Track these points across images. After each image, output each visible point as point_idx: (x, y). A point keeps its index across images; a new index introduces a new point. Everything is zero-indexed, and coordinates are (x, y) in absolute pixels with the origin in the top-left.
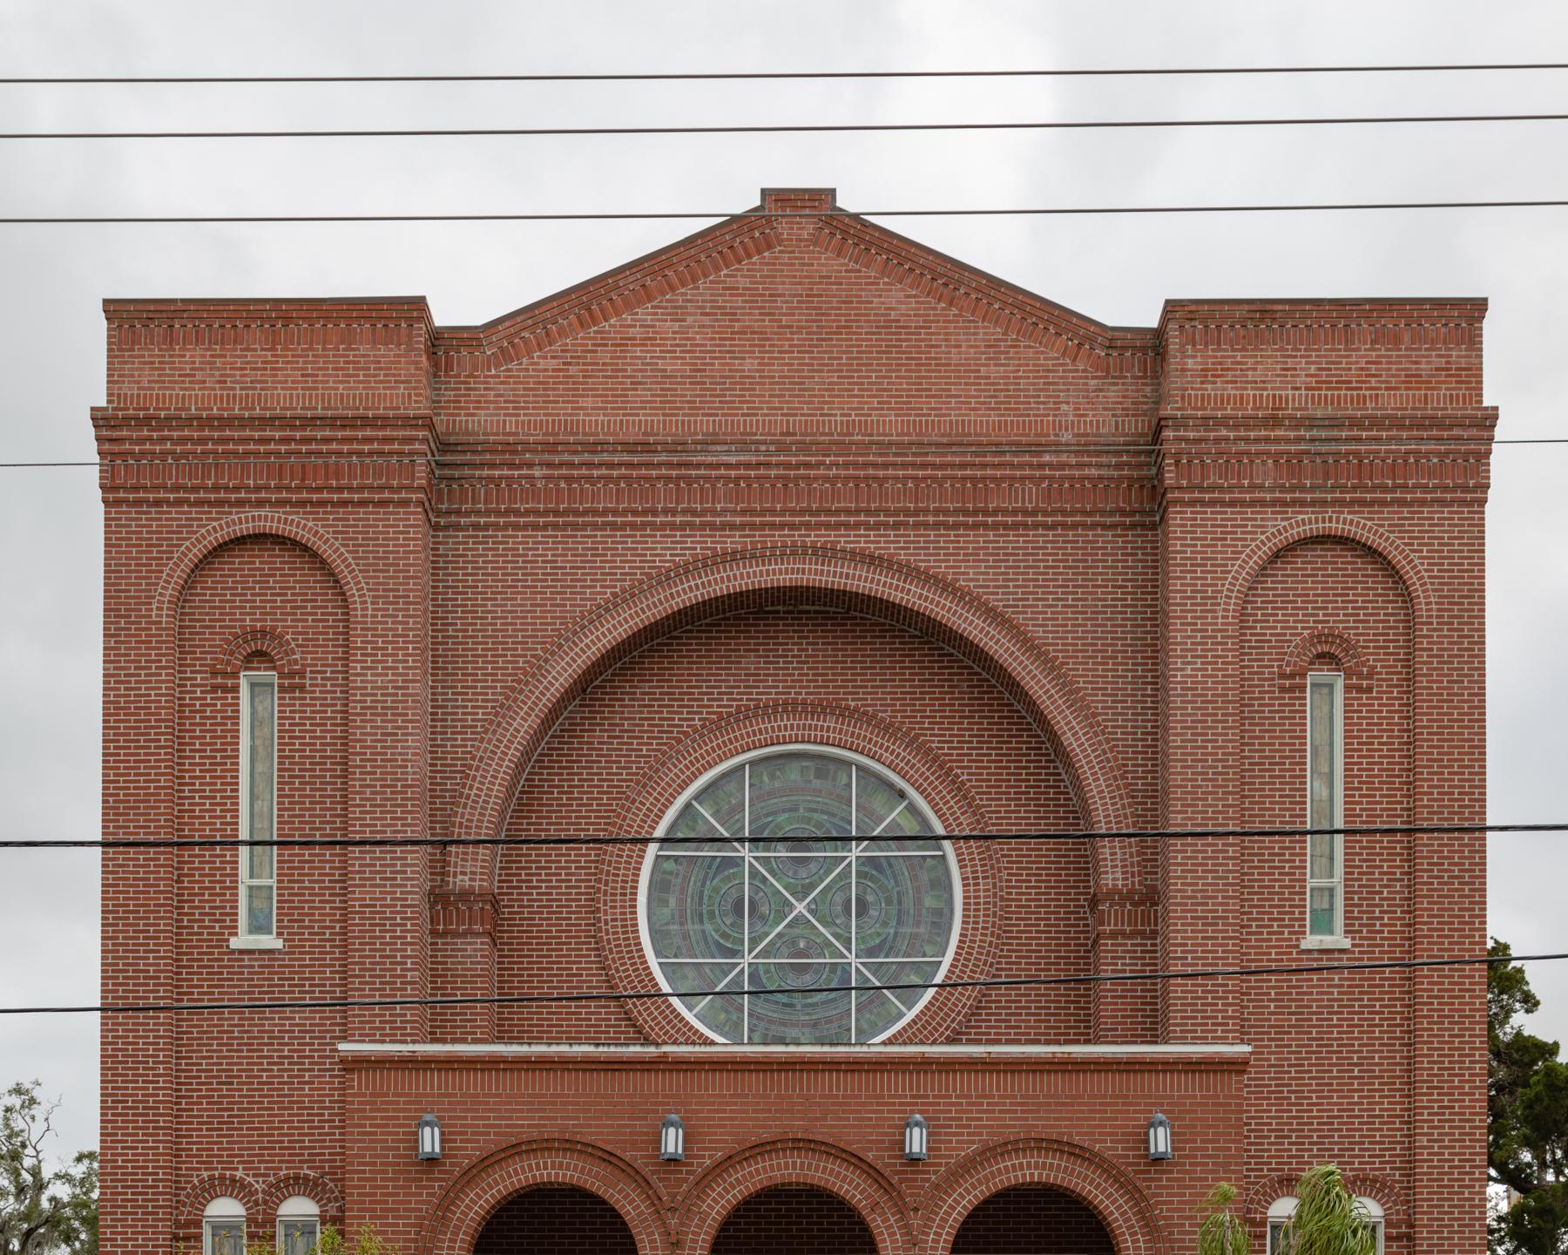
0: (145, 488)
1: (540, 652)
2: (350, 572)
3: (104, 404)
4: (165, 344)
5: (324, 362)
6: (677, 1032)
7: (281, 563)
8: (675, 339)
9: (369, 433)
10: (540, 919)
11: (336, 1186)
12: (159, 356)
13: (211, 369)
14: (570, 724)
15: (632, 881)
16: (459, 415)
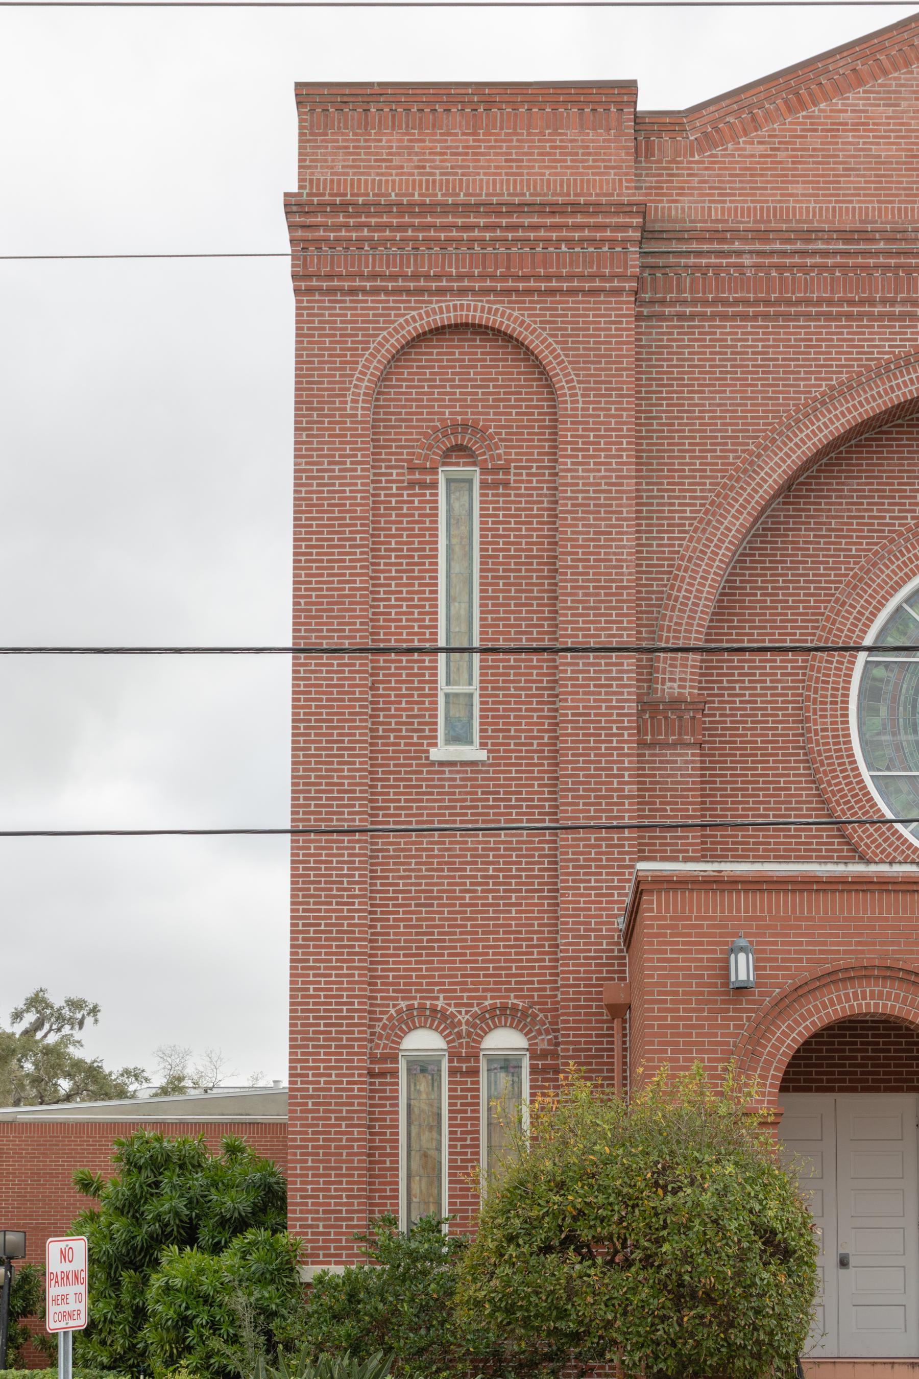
0: (340, 276)
1: (752, 447)
2: (559, 364)
3: (294, 189)
4: (359, 128)
5: (529, 147)
6: (895, 850)
7: (482, 353)
8: (889, 124)
9: (579, 219)
10: (744, 729)
11: (546, 1017)
12: (353, 141)
13: (409, 154)
14: (773, 523)
15: (843, 688)
16: (661, 201)
